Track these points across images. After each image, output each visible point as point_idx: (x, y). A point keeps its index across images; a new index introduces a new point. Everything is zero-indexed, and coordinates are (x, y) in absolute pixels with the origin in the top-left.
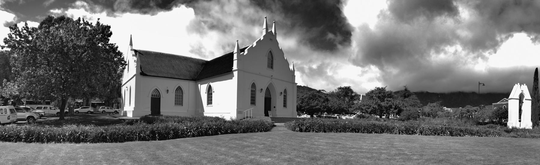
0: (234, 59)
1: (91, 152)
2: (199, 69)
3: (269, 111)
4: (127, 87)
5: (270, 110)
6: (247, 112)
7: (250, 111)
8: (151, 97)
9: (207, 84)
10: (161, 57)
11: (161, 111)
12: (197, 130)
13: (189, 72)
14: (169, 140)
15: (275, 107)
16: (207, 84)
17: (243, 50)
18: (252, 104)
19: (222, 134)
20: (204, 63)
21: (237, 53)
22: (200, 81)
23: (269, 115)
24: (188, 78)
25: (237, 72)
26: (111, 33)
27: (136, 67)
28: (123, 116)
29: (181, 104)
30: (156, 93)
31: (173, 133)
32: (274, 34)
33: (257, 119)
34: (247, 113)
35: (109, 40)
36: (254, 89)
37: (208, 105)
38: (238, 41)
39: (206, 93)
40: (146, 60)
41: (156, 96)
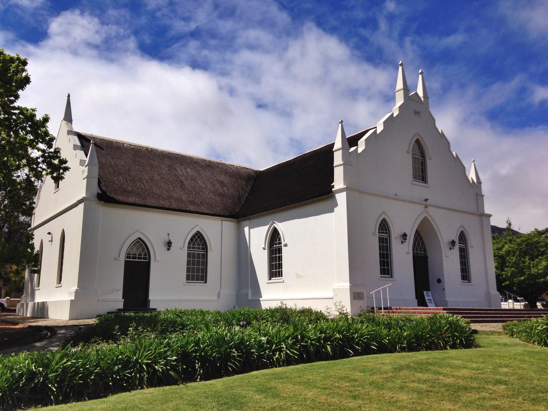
0: (335, 164)
1: (351, 401)
2: (242, 188)
3: (425, 292)
4: (49, 233)
5: (428, 289)
6: (378, 293)
7: (384, 290)
8: (125, 261)
9: (268, 226)
10: (149, 158)
11: (151, 297)
12: (294, 344)
14: (230, 378)
15: (439, 281)
16: (268, 226)
17: (353, 141)
18: (384, 274)
19: (357, 353)
20: (253, 176)
21: (343, 148)
22: (249, 219)
23: (427, 301)
24: (217, 210)
25: (344, 194)
26: (27, 80)
27: (87, 177)
28: (34, 317)
29: (203, 278)
30: (138, 248)
31: (238, 356)
32: (422, 99)
33: (404, 313)
34: (378, 299)
35: (17, 97)
36: (385, 236)
37: (270, 279)
38: (342, 122)
39: (264, 249)
40: (112, 162)
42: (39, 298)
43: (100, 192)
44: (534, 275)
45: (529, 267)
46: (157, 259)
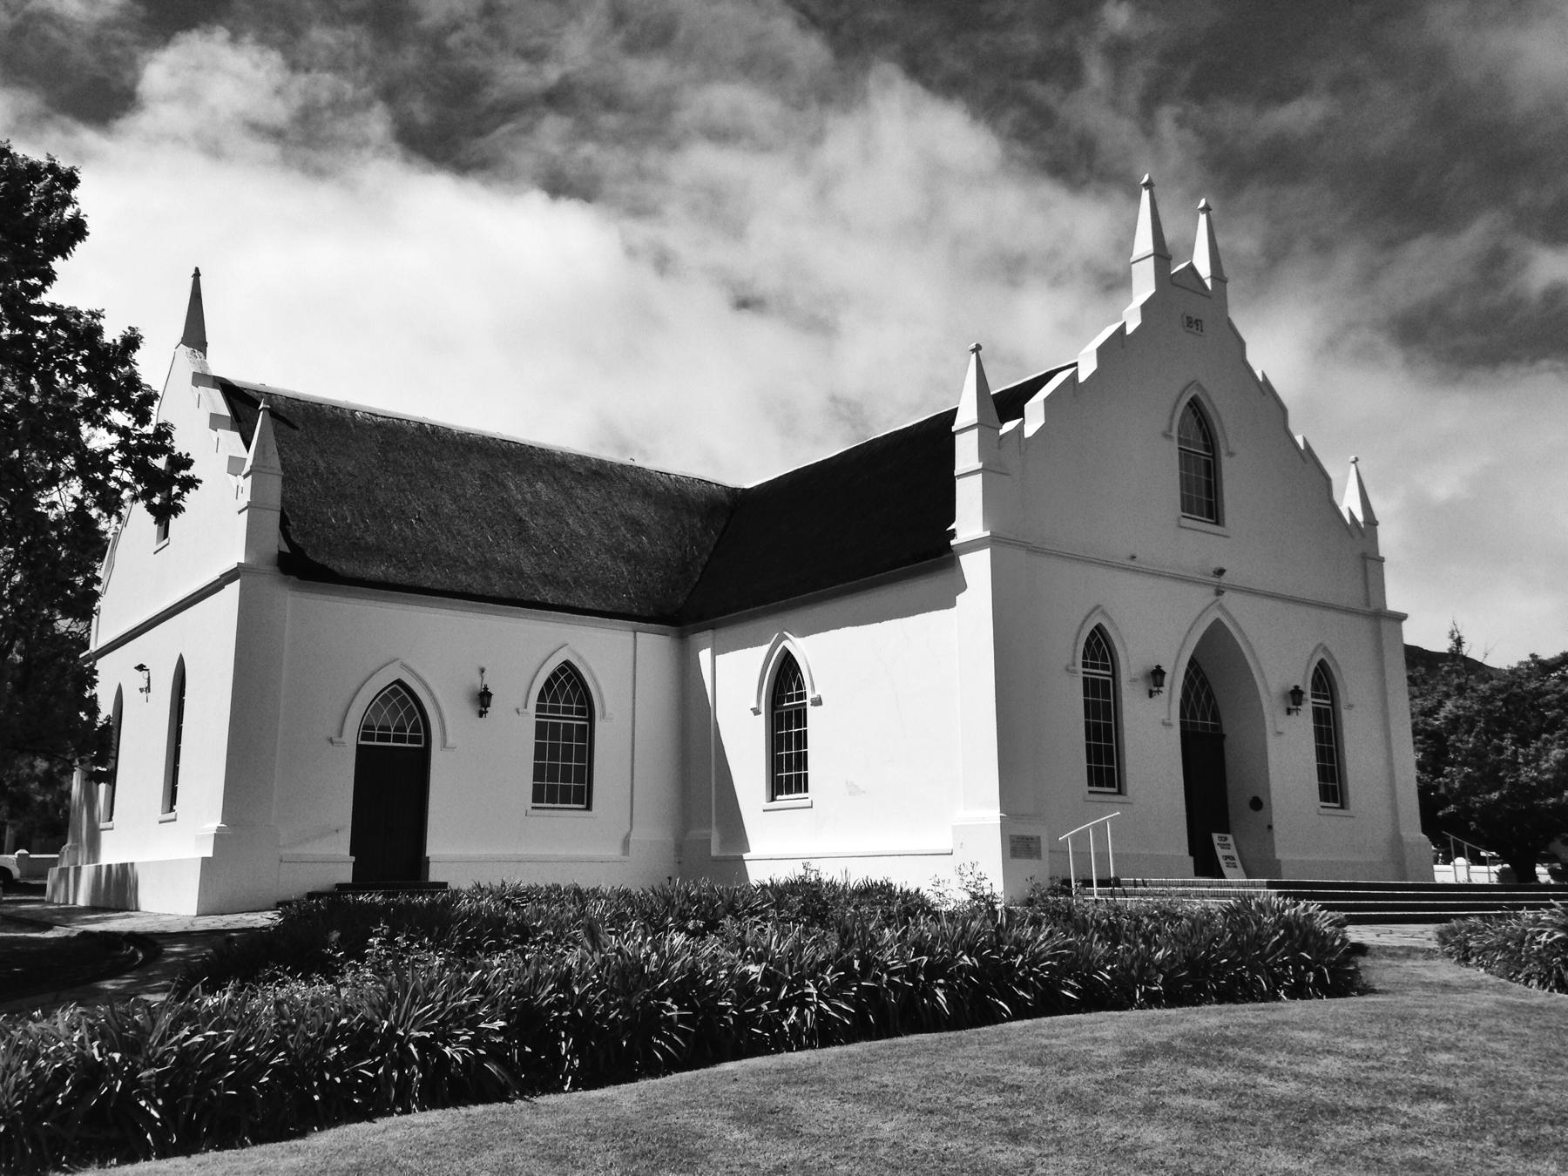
0: (959, 469)
3: (1215, 837)
6: (1080, 839)
7: (1100, 830)
8: (359, 747)
9: (766, 648)
10: (426, 452)
11: (431, 851)
13: (627, 561)
14: (657, 1081)
15: (1257, 804)
16: (766, 648)
17: (1010, 404)
18: (1100, 784)
19: (1022, 1011)
21: (981, 424)
22: (713, 627)
23: (1223, 863)
25: (985, 555)
27: (249, 506)
28: (98, 907)
31: (681, 1019)
33: (1155, 895)
34: (1082, 856)
36: (1101, 674)
37: (773, 799)
38: (977, 349)
39: (756, 712)
40: (322, 464)
41: (398, 739)
42: (112, 853)
43: (286, 549)
44: (1526, 786)
45: (1513, 765)
46: (450, 741)
